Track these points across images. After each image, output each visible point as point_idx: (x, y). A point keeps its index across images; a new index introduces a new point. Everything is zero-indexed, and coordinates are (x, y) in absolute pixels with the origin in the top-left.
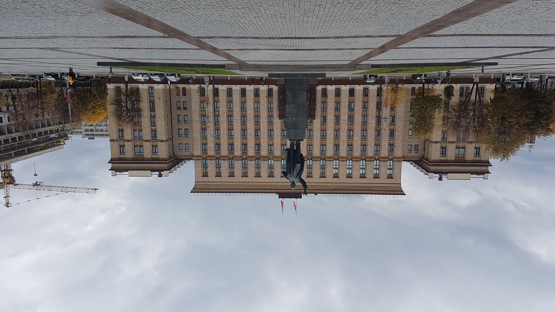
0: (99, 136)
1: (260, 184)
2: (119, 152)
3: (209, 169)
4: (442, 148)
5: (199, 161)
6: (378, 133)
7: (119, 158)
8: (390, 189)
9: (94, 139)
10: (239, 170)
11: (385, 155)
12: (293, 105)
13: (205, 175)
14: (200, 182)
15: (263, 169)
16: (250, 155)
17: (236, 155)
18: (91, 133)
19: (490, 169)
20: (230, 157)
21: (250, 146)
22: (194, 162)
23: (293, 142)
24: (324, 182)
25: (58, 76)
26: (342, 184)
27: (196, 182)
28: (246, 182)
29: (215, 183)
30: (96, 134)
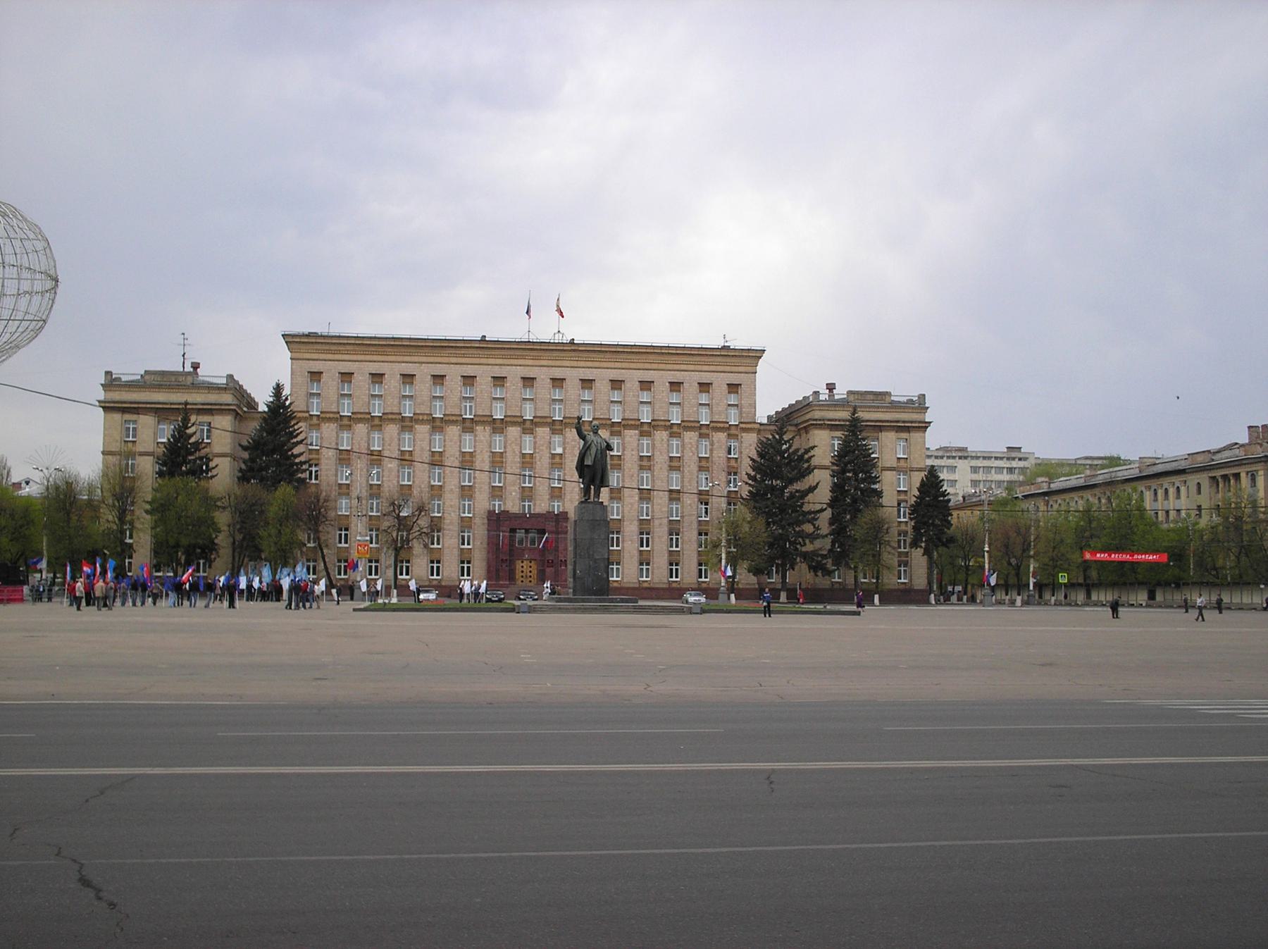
0: (993, 455)
1: (612, 365)
7: (909, 433)
8: (319, 347)
9: (1008, 448)
10: (660, 397)
11: (328, 428)
14: (746, 373)
15: (605, 398)
16: (634, 431)
17: (664, 432)
18: (1015, 464)
19: (101, 395)
21: (633, 453)
22: (757, 416)
23: (596, 500)
24: (465, 366)
25: (397, 593)
26: (424, 359)
27: (753, 373)
28: (643, 369)
30: (1001, 462)
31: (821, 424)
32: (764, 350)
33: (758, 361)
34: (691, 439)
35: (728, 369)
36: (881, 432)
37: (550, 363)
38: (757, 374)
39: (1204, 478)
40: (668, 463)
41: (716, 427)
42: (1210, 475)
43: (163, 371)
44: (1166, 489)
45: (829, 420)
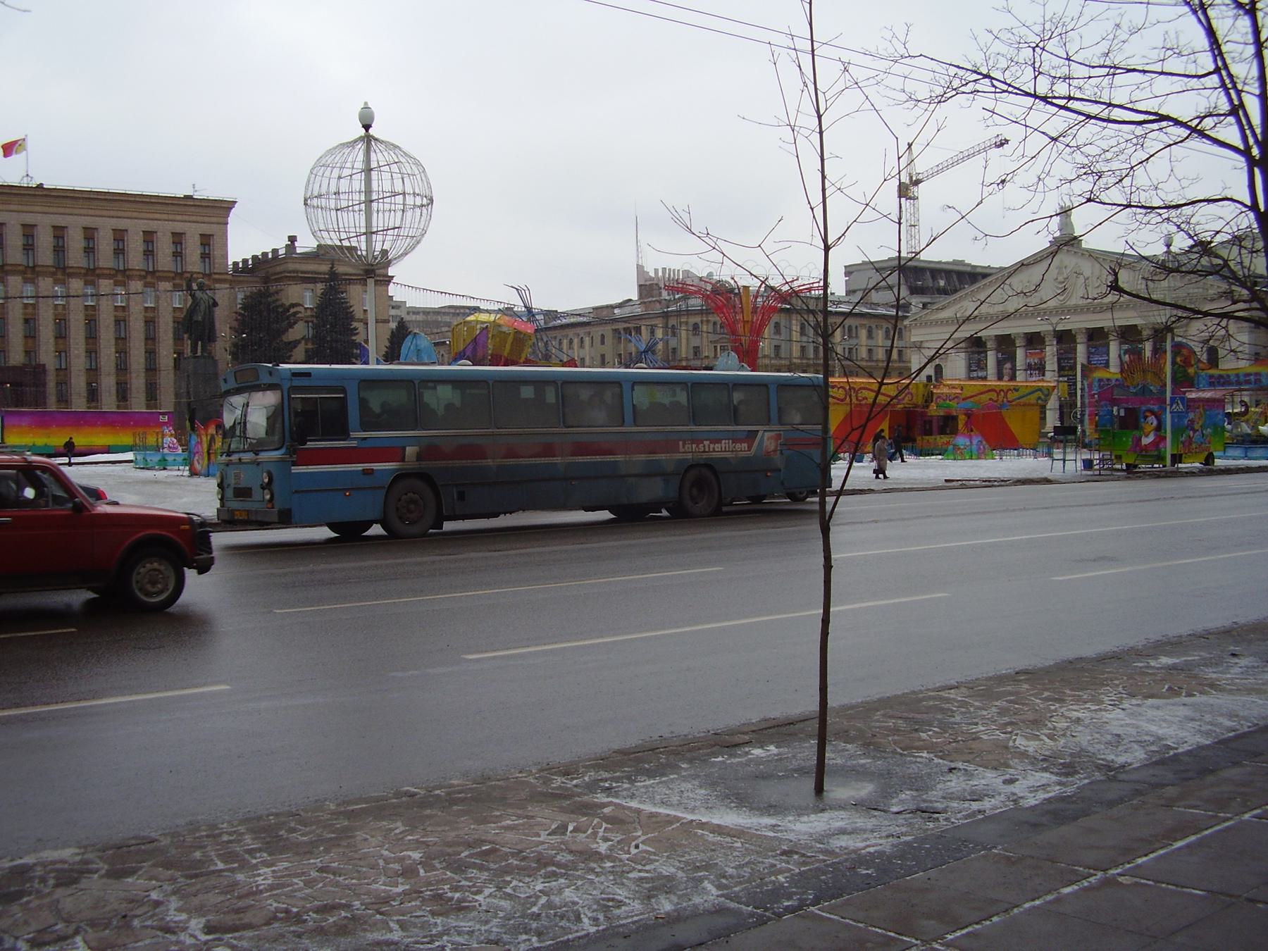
3: (199, 252)
4: (801, 347)
6: (122, 368)
13: (206, 240)
20: (209, 280)
29: (186, 218)
31: (295, 277)
32: (236, 202)
33: (230, 212)
35: (199, 219)
37: (20, 208)
39: (607, 330)
40: (143, 314)
42: (613, 327)
44: (571, 339)
45: (302, 272)
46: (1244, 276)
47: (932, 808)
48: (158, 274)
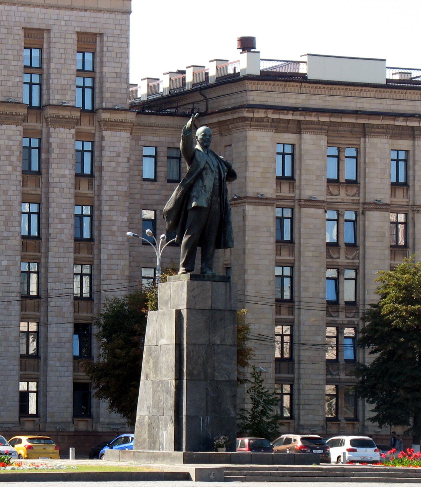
2: (411, 163)
5: (110, 106)
7: (299, 133)
12: (220, 379)
34: (9, 139)
36: (365, 136)
38: (131, 16)
41: (57, 117)
43: (129, 73)
46: (251, 421)
47: (316, 350)
48: (50, 112)
